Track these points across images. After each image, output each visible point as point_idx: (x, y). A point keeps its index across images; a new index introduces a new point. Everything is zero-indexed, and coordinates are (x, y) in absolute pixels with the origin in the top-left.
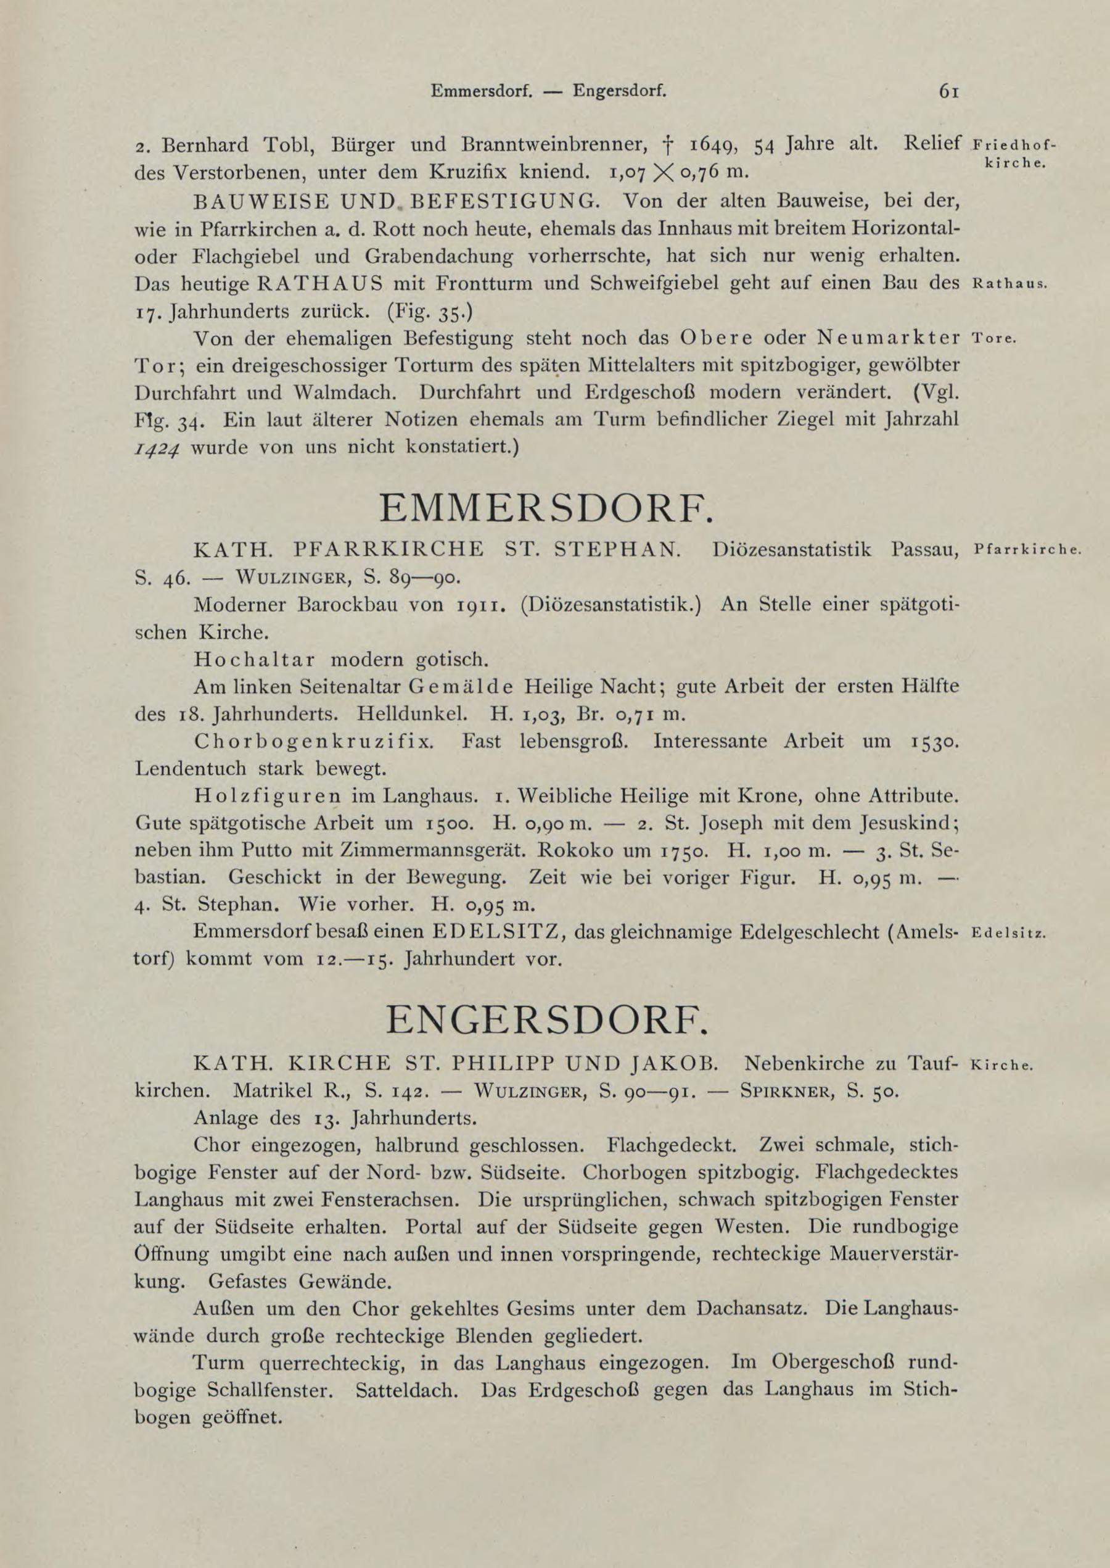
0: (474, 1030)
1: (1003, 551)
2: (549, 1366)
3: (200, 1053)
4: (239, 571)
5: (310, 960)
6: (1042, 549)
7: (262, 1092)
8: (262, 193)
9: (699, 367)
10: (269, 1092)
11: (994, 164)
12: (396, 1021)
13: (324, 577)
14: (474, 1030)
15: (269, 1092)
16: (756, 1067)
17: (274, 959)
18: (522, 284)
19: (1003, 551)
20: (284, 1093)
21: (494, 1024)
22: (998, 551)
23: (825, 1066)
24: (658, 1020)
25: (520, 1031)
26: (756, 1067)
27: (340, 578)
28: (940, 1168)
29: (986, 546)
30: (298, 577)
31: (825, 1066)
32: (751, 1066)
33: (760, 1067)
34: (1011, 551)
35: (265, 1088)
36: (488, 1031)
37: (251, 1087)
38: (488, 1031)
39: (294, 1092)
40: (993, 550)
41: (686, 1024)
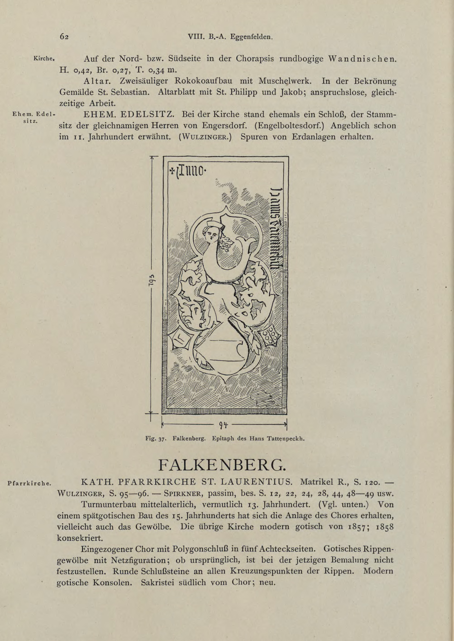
0: (281, 469)
1: (19, 484)
2: (371, 517)
3: (84, 478)
4: (59, 491)
5: (71, 137)
6: (21, 483)
7: (312, 482)
8: (63, 490)
9: (359, 516)
10: (315, 482)
11: (30, 484)
12: (162, 466)
13: (93, 494)
14: (281, 469)
15: (315, 482)
16: (116, 562)
17: (277, 137)
18: (216, 505)
19: (19, 484)
20: (321, 483)
21: (211, 467)
22: (17, 484)
23: (223, 115)
24: (264, 465)
25: (260, 469)
26: (116, 562)
27: (100, 494)
28: (294, 570)
29: (12, 482)
30: (83, 493)
31: (223, 115)
32: (114, 561)
33: (117, 561)
34: (23, 484)
35: (313, 481)
36: (247, 469)
37: (308, 480)
38: (247, 469)
39: (325, 483)
40: (15, 484)
41: (163, 467)
